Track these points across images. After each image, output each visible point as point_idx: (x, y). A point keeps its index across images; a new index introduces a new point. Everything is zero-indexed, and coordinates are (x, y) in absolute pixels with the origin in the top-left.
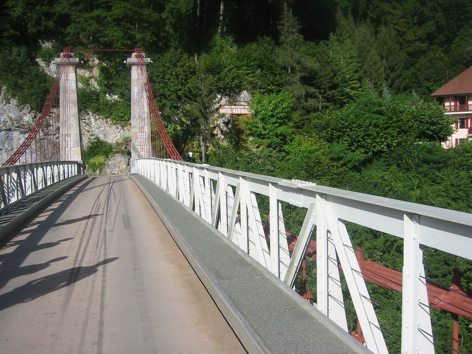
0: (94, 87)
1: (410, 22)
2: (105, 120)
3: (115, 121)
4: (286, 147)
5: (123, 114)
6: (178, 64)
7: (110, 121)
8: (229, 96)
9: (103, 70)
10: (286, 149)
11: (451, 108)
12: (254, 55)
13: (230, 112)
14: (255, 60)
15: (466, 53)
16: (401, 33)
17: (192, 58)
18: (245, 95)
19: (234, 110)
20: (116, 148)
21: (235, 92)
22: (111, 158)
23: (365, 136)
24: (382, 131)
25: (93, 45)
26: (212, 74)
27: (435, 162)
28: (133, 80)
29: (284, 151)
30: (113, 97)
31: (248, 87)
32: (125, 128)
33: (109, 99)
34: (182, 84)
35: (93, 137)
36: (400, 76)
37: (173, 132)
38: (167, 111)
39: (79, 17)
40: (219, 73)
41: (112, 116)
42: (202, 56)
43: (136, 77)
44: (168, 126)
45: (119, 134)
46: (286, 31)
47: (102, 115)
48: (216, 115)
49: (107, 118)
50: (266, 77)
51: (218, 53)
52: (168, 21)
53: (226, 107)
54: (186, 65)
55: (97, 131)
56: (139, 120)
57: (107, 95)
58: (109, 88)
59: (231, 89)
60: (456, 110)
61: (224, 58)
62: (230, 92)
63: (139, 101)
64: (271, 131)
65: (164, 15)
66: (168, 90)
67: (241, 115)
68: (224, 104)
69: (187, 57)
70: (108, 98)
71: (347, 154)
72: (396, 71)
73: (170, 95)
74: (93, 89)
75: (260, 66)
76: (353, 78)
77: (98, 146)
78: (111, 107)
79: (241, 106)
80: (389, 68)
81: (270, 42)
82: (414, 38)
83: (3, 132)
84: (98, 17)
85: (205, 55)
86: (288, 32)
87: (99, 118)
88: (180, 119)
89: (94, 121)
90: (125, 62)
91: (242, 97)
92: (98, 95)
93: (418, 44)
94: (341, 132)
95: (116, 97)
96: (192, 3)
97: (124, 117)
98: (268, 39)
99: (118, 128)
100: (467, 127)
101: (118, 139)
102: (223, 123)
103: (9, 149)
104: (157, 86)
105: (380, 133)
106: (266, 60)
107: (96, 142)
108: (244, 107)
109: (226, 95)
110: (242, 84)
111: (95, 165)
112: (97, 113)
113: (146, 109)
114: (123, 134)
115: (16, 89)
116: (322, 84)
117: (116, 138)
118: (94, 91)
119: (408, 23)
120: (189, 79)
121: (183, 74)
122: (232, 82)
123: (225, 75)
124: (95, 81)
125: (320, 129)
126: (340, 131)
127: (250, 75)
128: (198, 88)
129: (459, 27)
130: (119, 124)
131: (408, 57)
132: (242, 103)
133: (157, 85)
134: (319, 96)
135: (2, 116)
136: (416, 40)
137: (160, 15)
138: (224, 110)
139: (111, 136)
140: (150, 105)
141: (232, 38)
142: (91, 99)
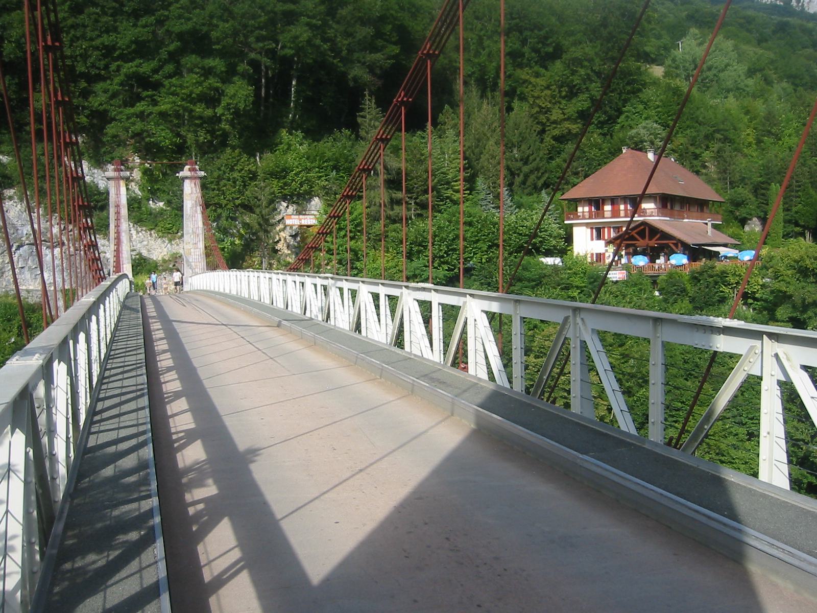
0: (135, 193)
1: (556, 95)
3: (160, 234)
4: (358, 264)
5: (170, 225)
8: (297, 203)
9: (145, 172)
11: (583, 215)
12: (329, 154)
13: (299, 224)
15: (629, 138)
16: (544, 110)
17: (252, 160)
20: (163, 266)
21: (304, 199)
24: (470, 245)
25: (133, 141)
26: (276, 178)
27: (529, 281)
29: (356, 268)
32: (173, 243)
33: (153, 207)
34: (240, 192)
35: (134, 253)
36: (538, 169)
37: (230, 247)
39: (121, 113)
40: (285, 177)
41: (157, 228)
45: (166, 249)
47: (145, 226)
51: (285, 152)
53: (293, 217)
55: (139, 245)
58: (153, 194)
59: (299, 195)
60: (590, 218)
61: (290, 159)
64: (342, 246)
65: (219, 111)
66: (224, 198)
67: (312, 226)
71: (425, 271)
72: (531, 163)
73: (226, 205)
74: (133, 195)
75: (335, 168)
77: (141, 263)
78: (156, 217)
80: (521, 160)
81: (351, 135)
82: (562, 117)
84: (142, 112)
85: (269, 154)
87: (142, 230)
88: (238, 231)
92: (140, 203)
93: (567, 125)
95: (161, 204)
98: (348, 132)
99: (164, 242)
100: (604, 239)
102: (290, 236)
103: (34, 267)
104: (212, 194)
105: (468, 247)
107: (138, 259)
109: (293, 203)
113: (200, 224)
114: (170, 249)
117: (162, 254)
118: (135, 197)
119: (553, 97)
127: (323, 179)
128: (256, 198)
129: (626, 101)
131: (554, 142)
132: (313, 212)
136: (565, 120)
141: (302, 132)
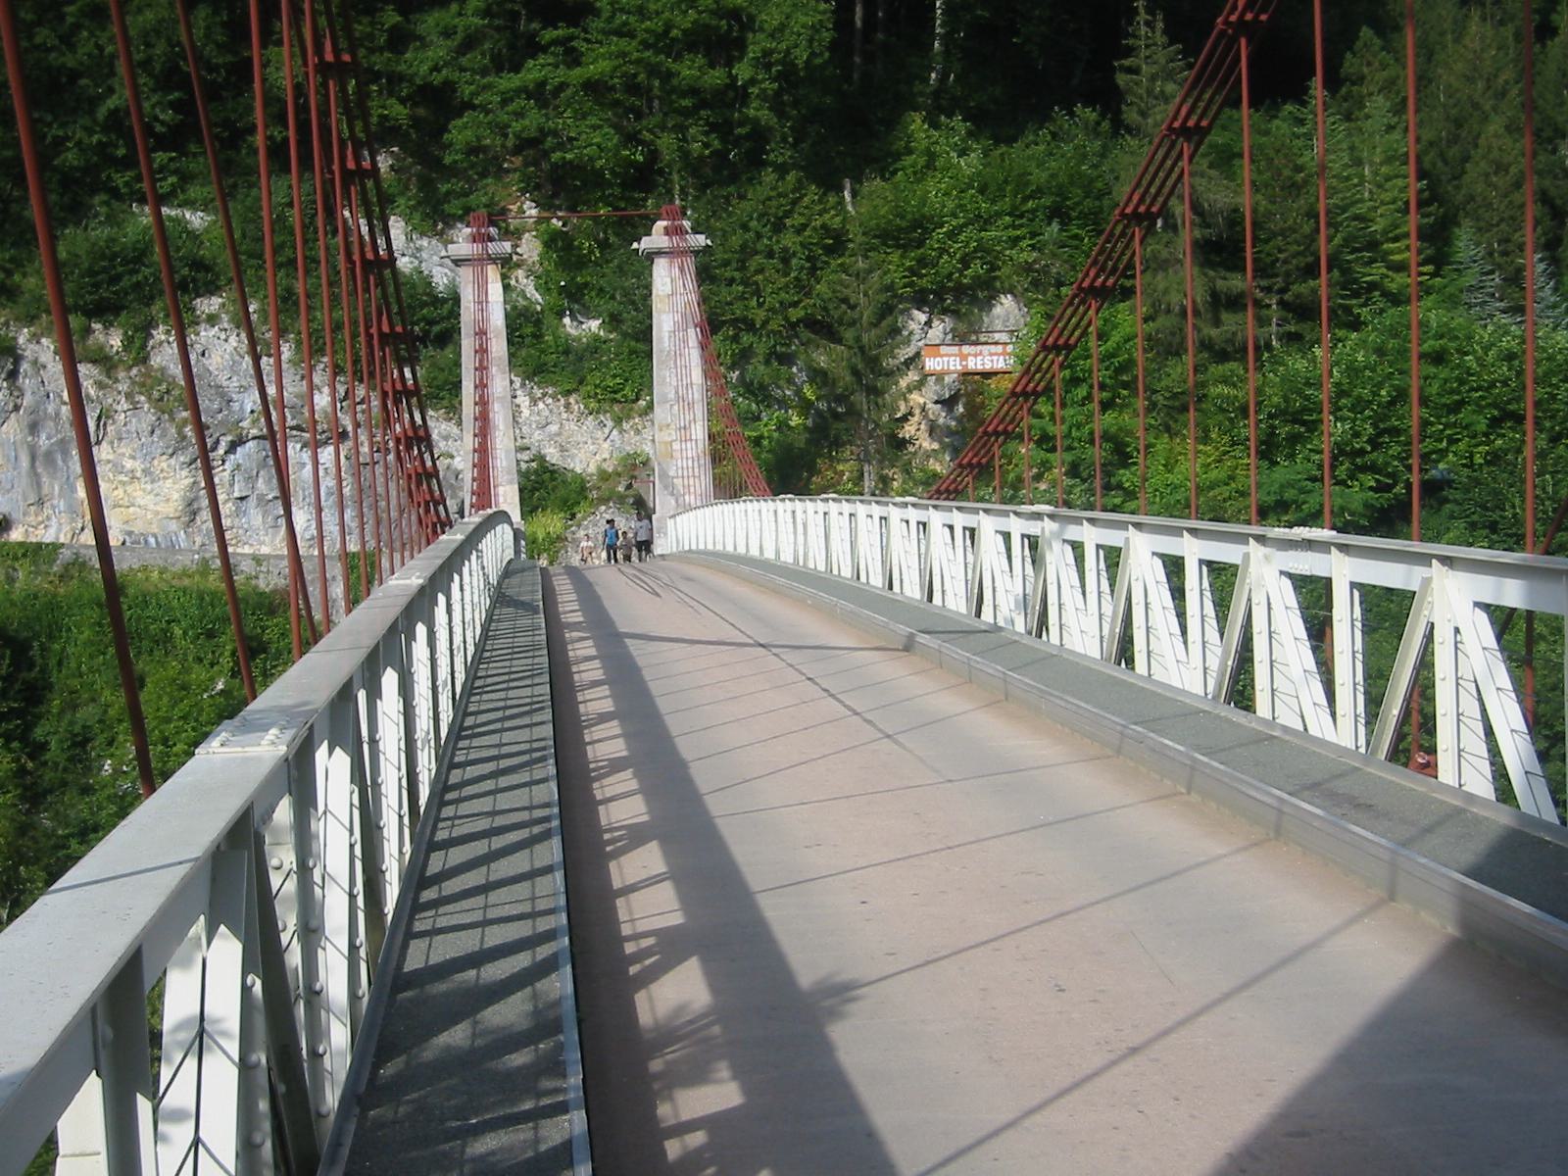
0: (525, 297)
2: (562, 401)
3: (593, 405)
6: (788, 222)
7: (577, 402)
8: (955, 313)
9: (553, 242)
10: (1124, 479)
13: (959, 368)
14: (1038, 193)
17: (832, 199)
18: (1006, 307)
19: (970, 358)
20: (599, 488)
22: (584, 519)
23: (1380, 434)
24: (1439, 417)
26: (898, 247)
28: (658, 295)
29: (1119, 486)
30: (584, 327)
31: (1018, 282)
33: (573, 332)
35: (525, 456)
38: (758, 370)
40: (920, 244)
41: (584, 389)
42: (866, 187)
43: (668, 289)
44: (759, 415)
45: (606, 445)
46: (1141, 91)
47: (554, 385)
48: (913, 376)
49: (568, 393)
50: (1077, 248)
51: (920, 176)
52: (754, 90)
53: (944, 350)
54: (813, 224)
55: (537, 435)
56: (676, 407)
57: (567, 320)
58: (575, 298)
59: (960, 291)
61: (934, 193)
62: (957, 300)
63: (678, 355)
65: (743, 71)
67: (996, 373)
68: (938, 342)
69: (816, 197)
70: (568, 329)
74: (522, 302)
75: (1057, 213)
76: (1398, 231)
78: (580, 359)
79: (993, 347)
81: (1098, 123)
83: (251, 444)
86: (1150, 92)
87: (544, 395)
88: (799, 392)
89: (527, 403)
90: (635, 245)
91: (998, 317)
92: (538, 323)
94: (1304, 423)
95: (594, 325)
96: (828, 30)
97: (622, 389)
98: (1090, 115)
101: (605, 460)
102: (936, 402)
103: (270, 497)
104: (725, 294)
105: (1432, 424)
106: (1079, 191)
107: (536, 472)
108: (1004, 349)
109: (945, 311)
110: (998, 273)
111: (533, 542)
112: (536, 379)
113: (697, 375)
115: (287, 310)
116: (1277, 260)
117: (598, 457)
118: (526, 308)
120: (822, 269)
121: (802, 254)
122: (961, 272)
123: (939, 248)
124: (527, 277)
125: (1233, 415)
126: (1294, 421)
127: (1024, 244)
128: (845, 300)
130: (606, 412)
132: (997, 336)
133: (724, 290)
134: (1268, 301)
135: (246, 395)
137: (730, 72)
138: (938, 359)
139: (583, 451)
140: (708, 374)
141: (964, 120)
142: (519, 336)
